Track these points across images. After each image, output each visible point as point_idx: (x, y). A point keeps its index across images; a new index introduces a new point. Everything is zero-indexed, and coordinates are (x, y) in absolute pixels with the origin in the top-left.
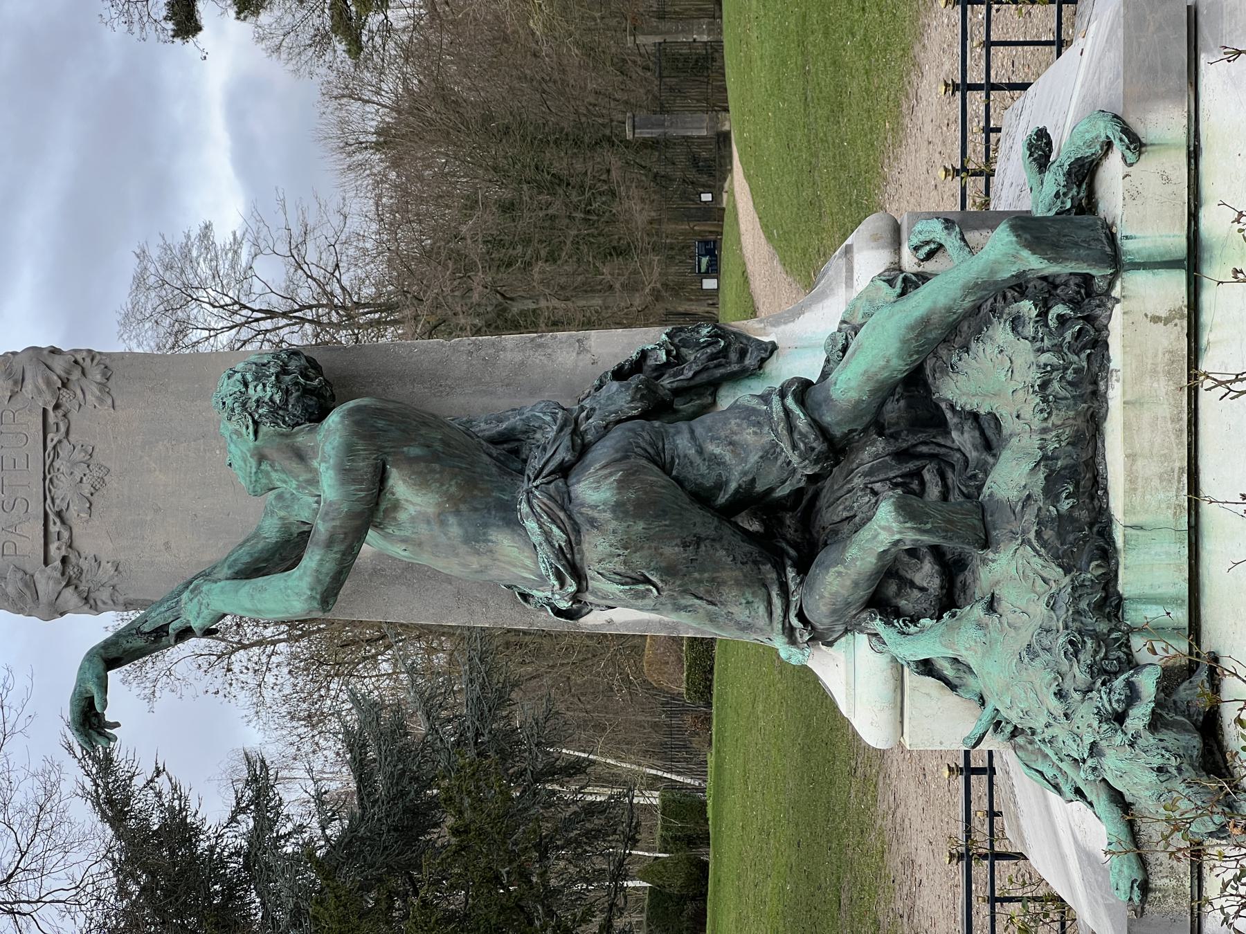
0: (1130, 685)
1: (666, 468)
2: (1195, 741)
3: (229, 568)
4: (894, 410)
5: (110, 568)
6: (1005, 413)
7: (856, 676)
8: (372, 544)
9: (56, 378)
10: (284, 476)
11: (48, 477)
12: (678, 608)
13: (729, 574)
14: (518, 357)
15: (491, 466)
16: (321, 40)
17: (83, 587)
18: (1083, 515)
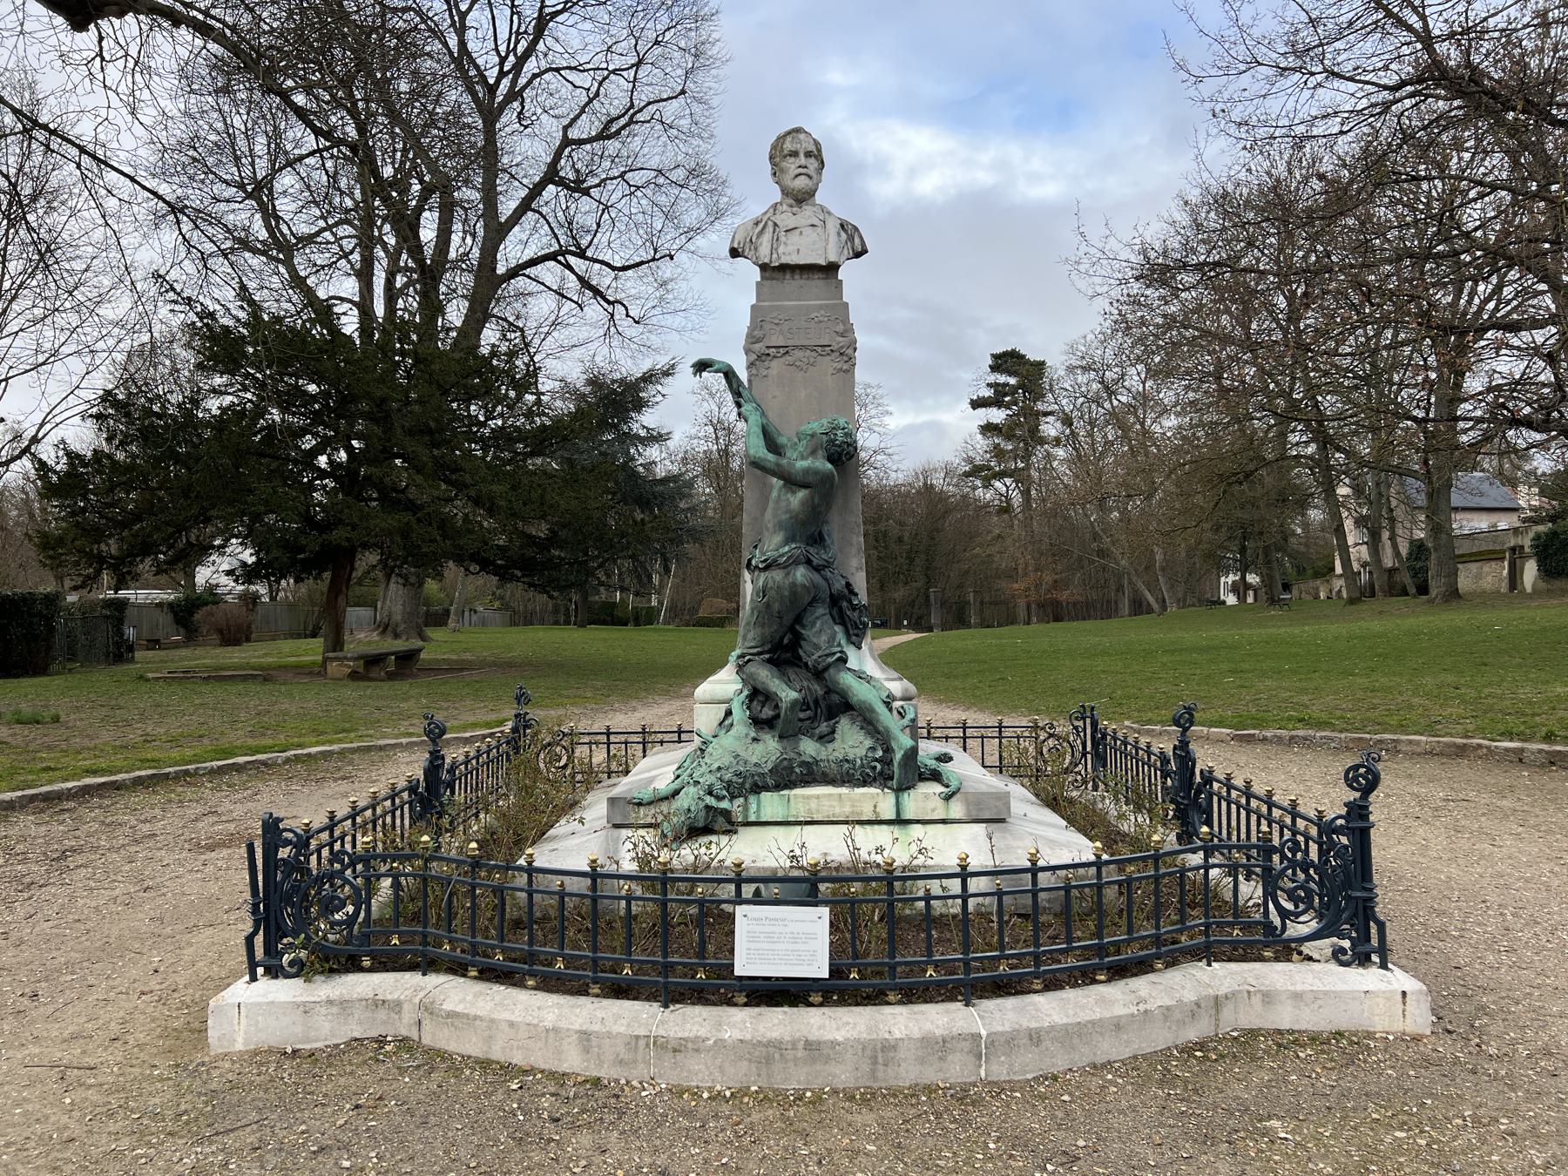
0: (724, 797)
1: (810, 604)
2: (701, 824)
4: (835, 698)
6: (836, 745)
7: (724, 683)
8: (777, 483)
12: (753, 610)
13: (767, 631)
15: (810, 531)
16: (970, 460)
18: (793, 777)
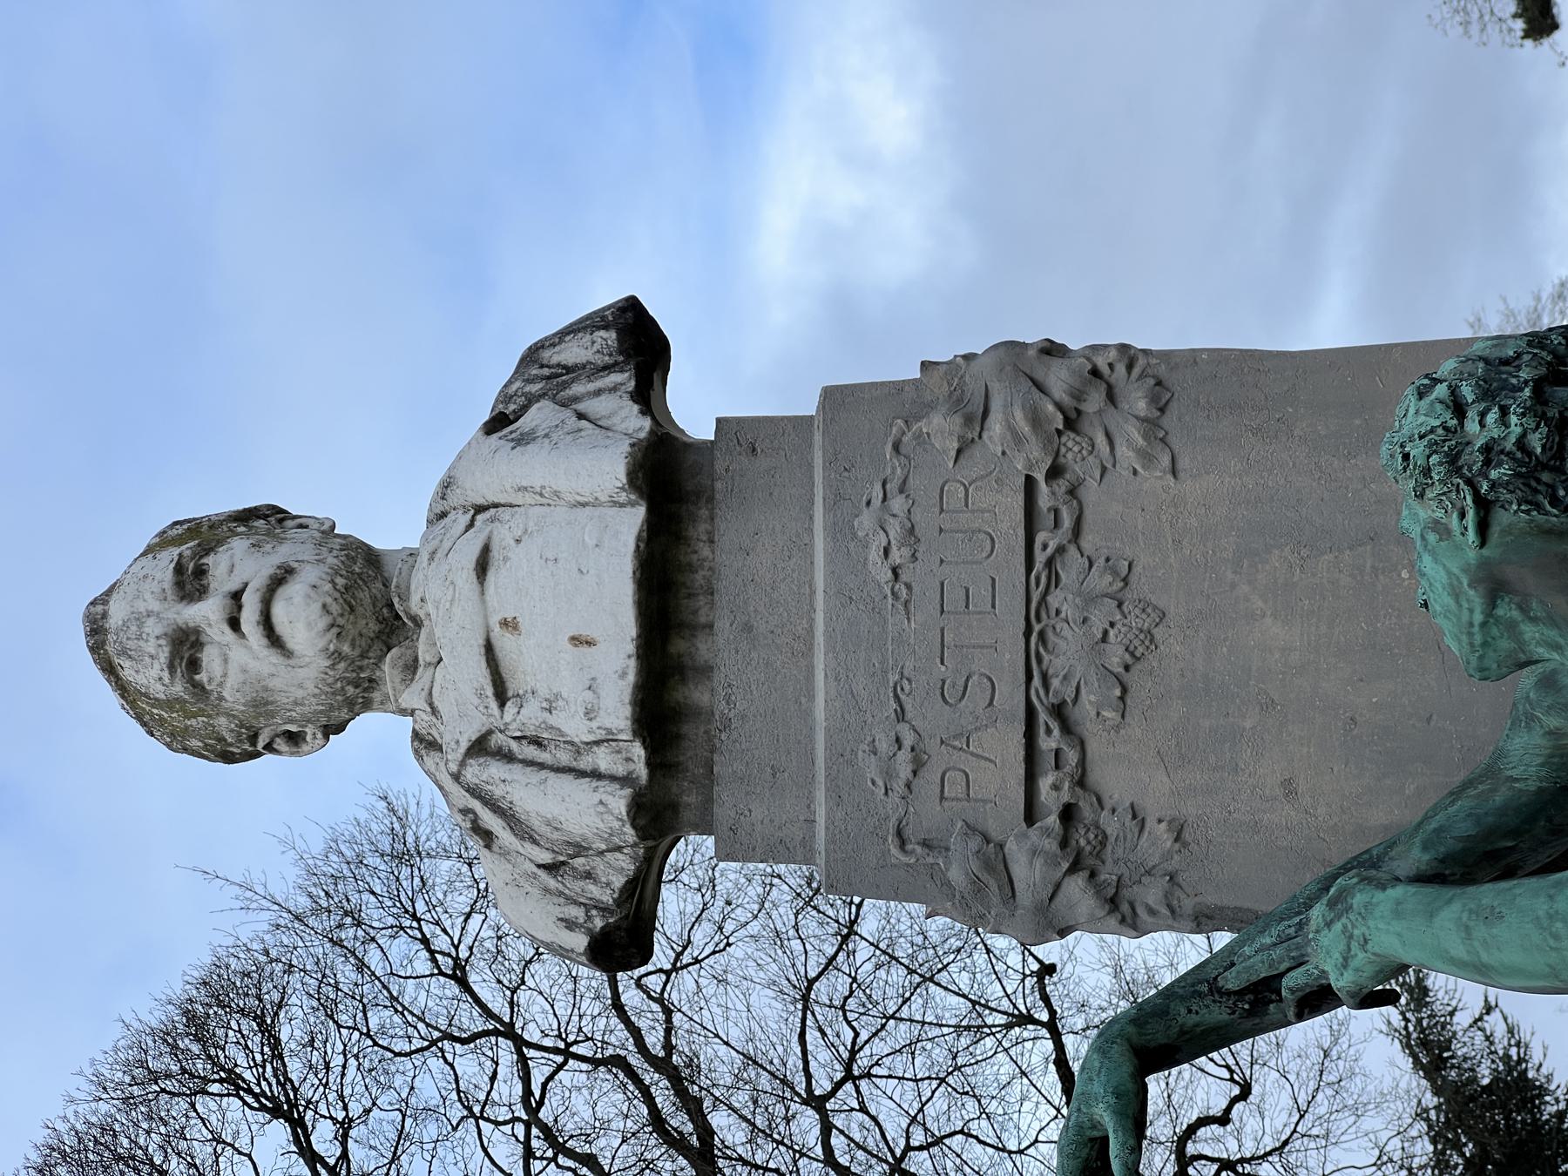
3: (1425, 848)
5: (1161, 833)
9: (1051, 408)
10: (1552, 634)
11: (1037, 628)
17: (1107, 875)
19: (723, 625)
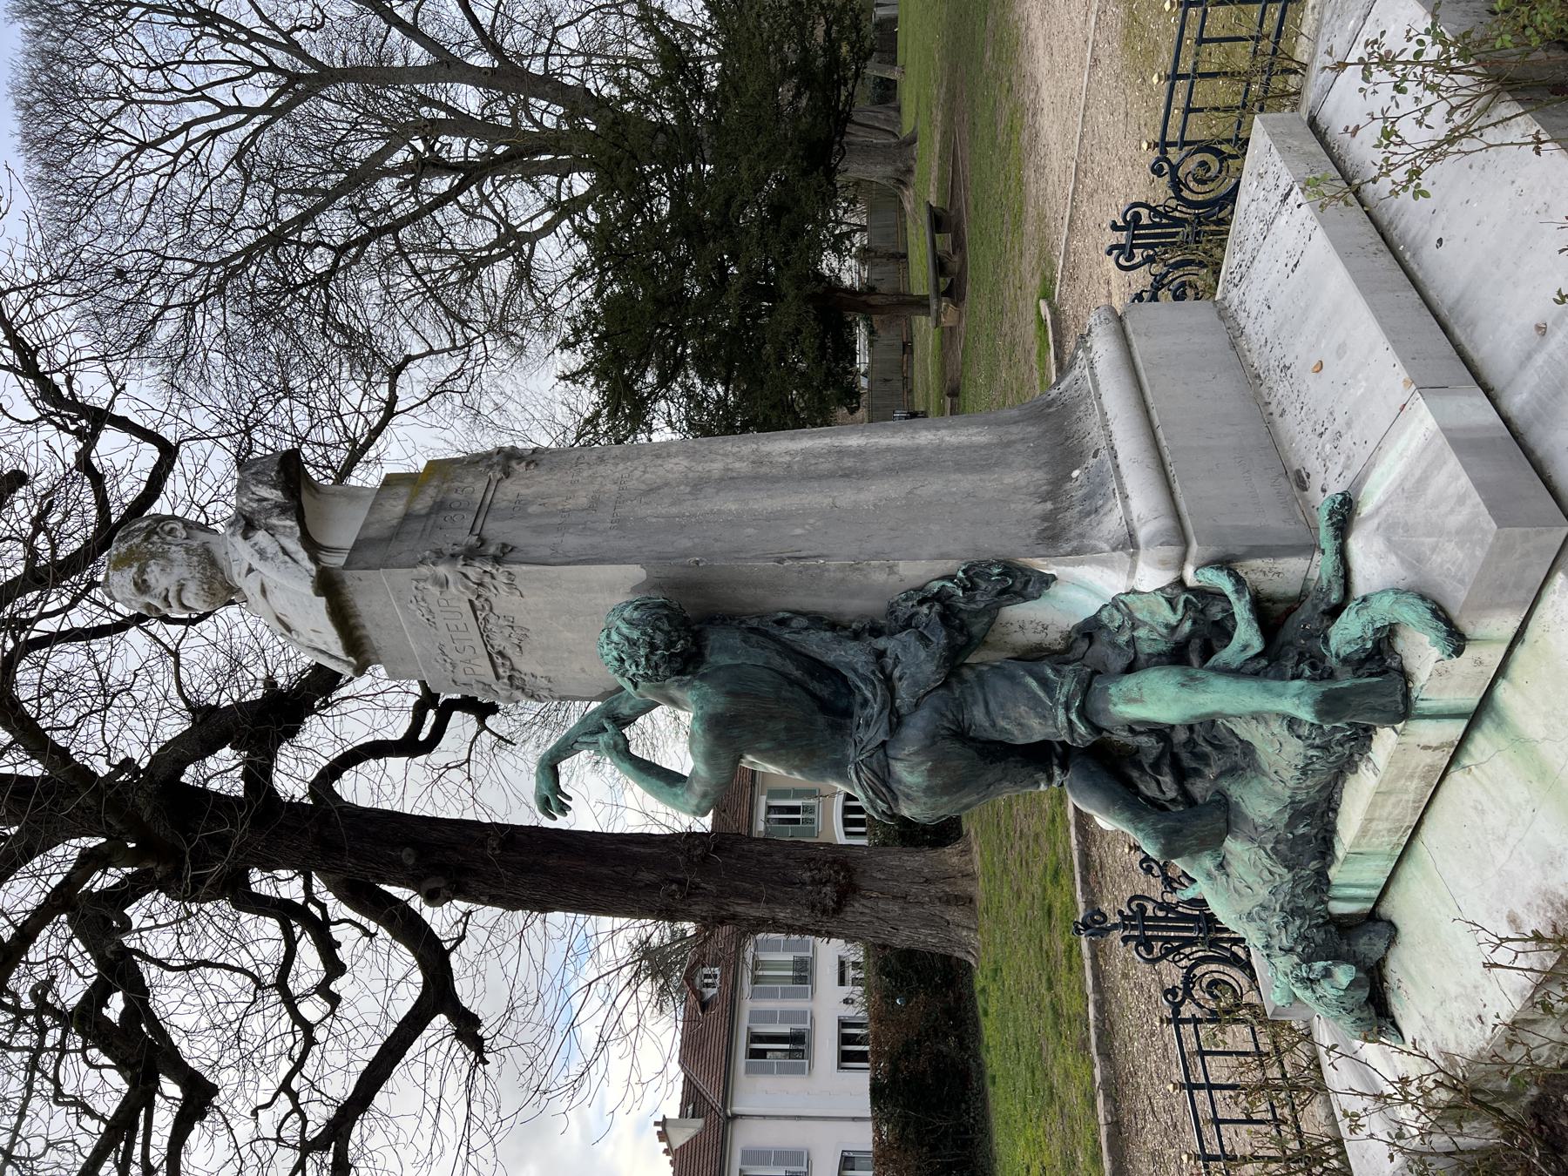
14: (839, 575)
19: (368, 625)
